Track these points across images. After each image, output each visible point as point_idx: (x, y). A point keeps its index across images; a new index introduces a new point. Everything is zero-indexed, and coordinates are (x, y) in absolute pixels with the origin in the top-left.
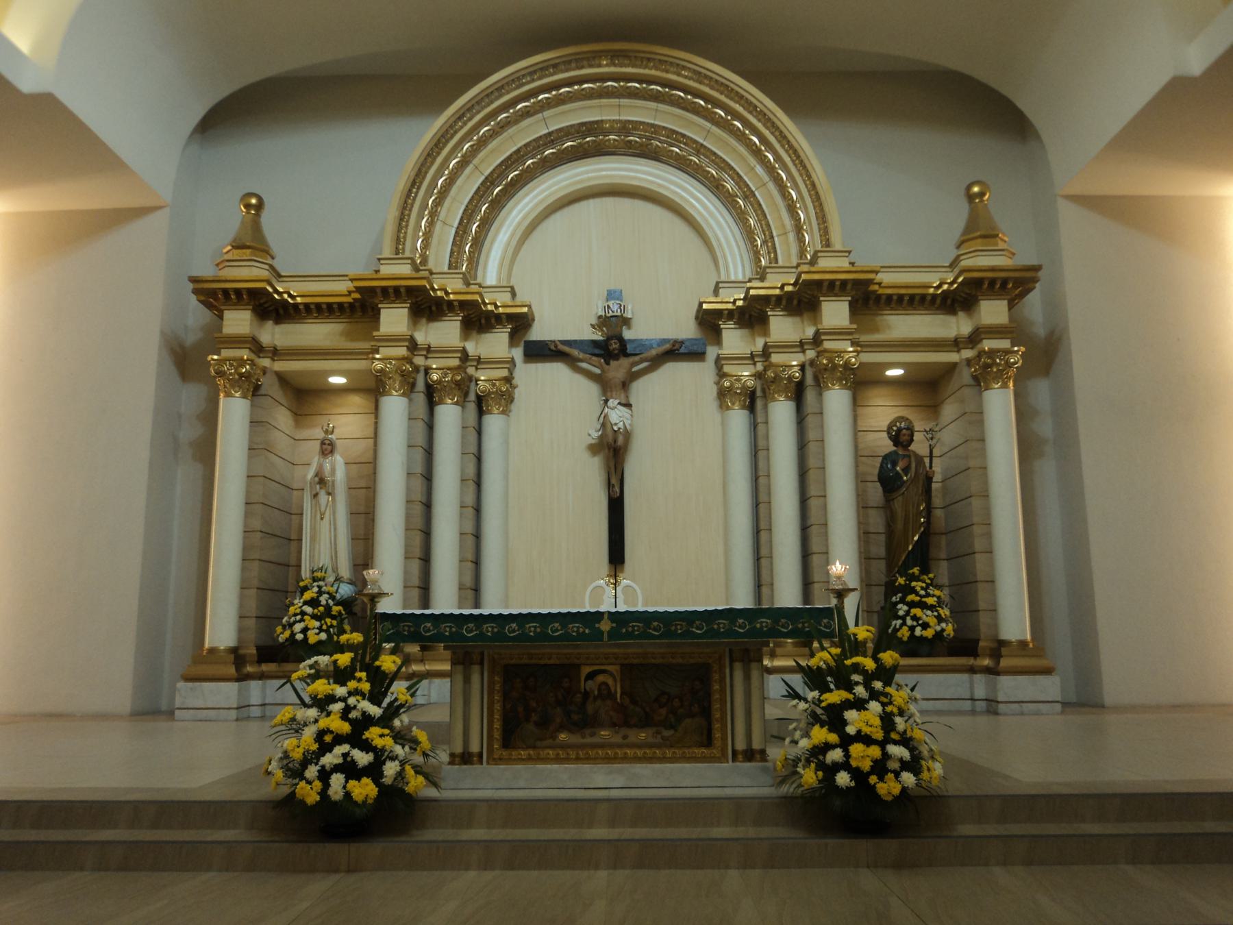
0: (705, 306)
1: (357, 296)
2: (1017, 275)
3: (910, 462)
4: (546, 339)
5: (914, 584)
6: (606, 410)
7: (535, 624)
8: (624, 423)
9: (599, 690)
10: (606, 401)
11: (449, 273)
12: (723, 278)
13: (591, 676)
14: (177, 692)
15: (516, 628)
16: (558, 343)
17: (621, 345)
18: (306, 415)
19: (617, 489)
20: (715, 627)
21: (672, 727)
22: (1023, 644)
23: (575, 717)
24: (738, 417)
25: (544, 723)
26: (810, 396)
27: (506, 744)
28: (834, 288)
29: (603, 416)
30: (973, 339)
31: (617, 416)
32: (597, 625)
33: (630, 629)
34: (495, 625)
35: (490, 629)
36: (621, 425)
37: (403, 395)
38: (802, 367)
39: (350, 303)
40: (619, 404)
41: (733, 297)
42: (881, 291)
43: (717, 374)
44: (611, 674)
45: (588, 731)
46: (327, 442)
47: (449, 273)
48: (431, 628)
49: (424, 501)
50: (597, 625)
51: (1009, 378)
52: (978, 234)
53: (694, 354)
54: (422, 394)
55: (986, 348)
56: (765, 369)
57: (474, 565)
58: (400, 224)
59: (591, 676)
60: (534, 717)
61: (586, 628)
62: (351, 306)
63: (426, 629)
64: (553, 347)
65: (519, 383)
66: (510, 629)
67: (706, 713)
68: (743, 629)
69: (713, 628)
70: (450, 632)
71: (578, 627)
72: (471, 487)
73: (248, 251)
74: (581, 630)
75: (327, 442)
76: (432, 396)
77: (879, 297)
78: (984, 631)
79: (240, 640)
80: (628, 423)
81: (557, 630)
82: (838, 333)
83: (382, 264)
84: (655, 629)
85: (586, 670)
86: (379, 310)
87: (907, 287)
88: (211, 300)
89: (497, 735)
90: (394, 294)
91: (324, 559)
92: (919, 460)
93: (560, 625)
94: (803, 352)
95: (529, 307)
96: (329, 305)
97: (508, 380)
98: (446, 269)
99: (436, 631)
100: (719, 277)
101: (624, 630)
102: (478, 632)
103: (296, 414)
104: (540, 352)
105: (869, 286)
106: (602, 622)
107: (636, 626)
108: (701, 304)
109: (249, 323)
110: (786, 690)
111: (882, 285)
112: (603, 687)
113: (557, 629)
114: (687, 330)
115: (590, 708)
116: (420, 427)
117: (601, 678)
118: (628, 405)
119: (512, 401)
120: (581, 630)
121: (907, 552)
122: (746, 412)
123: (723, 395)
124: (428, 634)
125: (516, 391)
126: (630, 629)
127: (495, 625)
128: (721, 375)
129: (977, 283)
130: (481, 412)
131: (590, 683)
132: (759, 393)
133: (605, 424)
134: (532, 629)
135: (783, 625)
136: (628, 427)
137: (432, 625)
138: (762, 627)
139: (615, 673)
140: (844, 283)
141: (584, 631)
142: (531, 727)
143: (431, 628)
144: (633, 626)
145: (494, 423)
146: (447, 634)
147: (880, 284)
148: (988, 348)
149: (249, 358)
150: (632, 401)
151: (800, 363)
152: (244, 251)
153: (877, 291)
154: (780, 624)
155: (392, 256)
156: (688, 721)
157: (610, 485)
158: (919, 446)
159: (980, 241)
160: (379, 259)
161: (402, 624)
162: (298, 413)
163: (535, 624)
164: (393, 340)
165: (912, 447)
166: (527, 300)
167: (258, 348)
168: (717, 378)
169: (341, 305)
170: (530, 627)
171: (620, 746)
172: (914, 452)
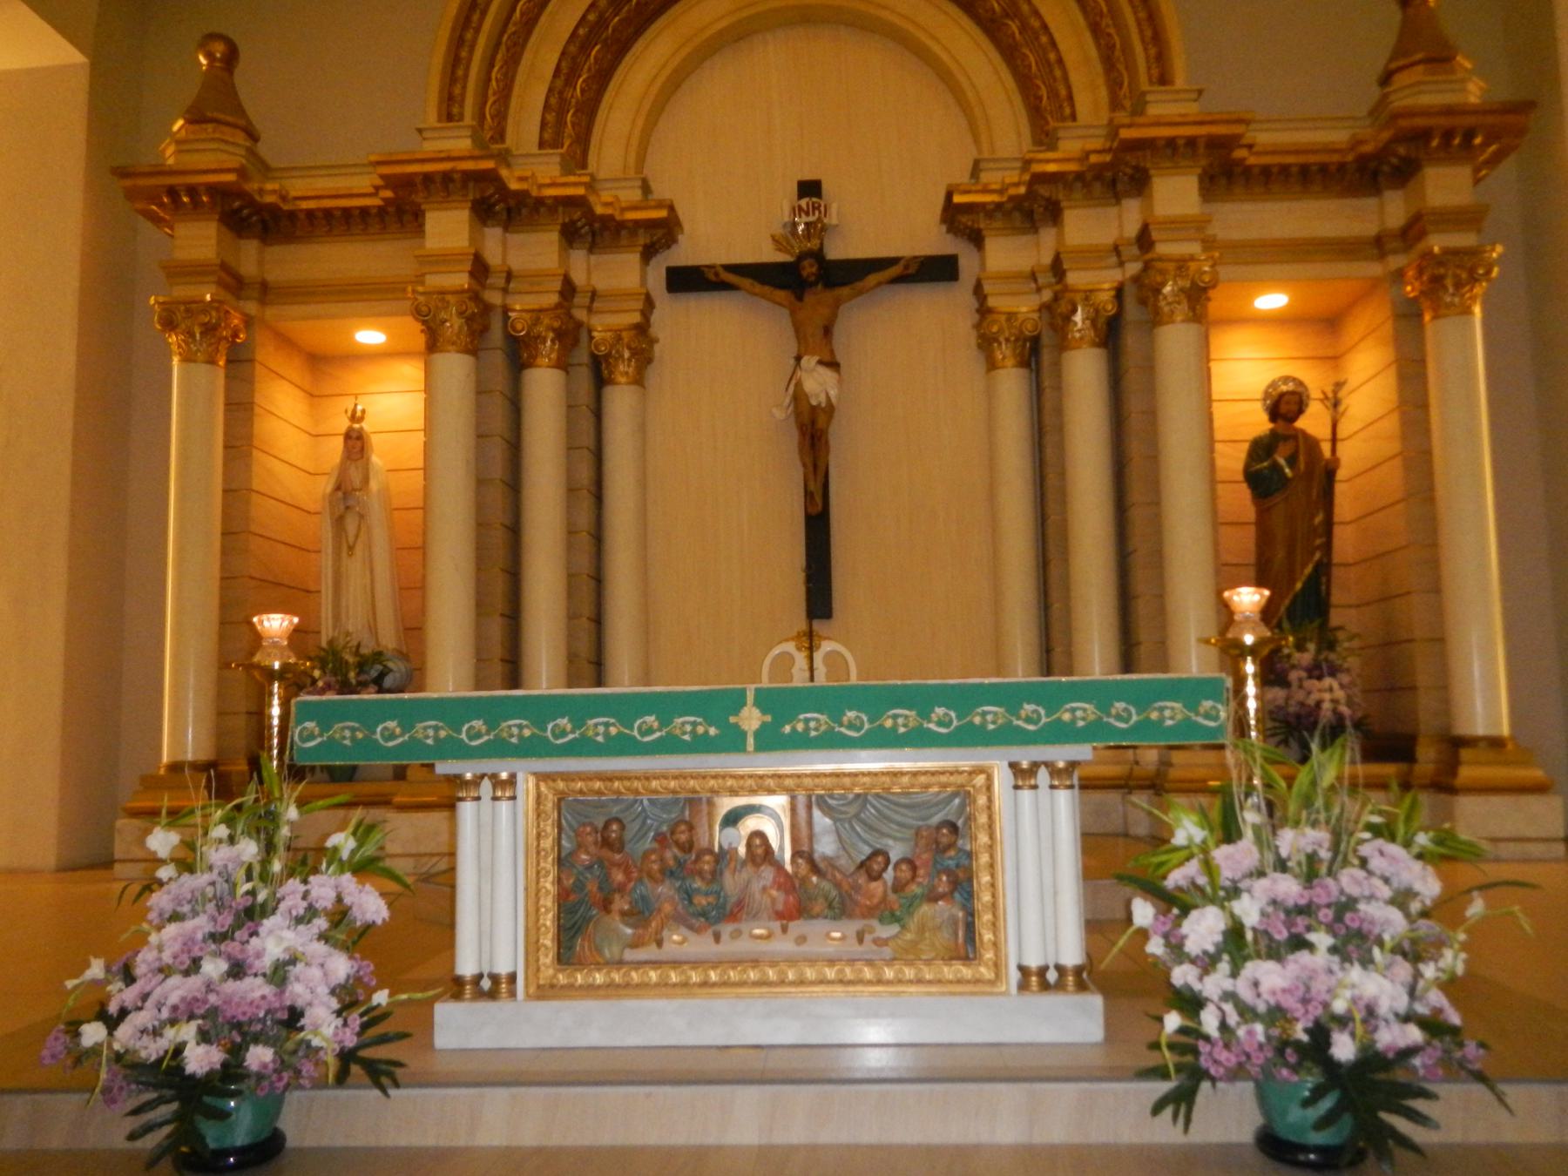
0: (957, 199)
1: (388, 194)
2: (1490, 120)
3: (1297, 447)
4: (700, 263)
5: (615, 797)
6: (799, 373)
7: (605, 719)
8: (827, 394)
9: (749, 845)
10: (798, 359)
11: (540, 155)
12: (986, 155)
13: (733, 818)
14: (116, 835)
15: (569, 727)
16: (721, 271)
17: (820, 268)
18: (327, 396)
19: (818, 499)
20: (977, 720)
21: (894, 918)
22: (1496, 743)
23: (701, 901)
24: (1011, 384)
25: (640, 914)
26: (1131, 340)
27: (566, 956)
28: (1174, 150)
29: (793, 382)
30: (1412, 232)
31: (818, 383)
32: (732, 720)
33: (800, 727)
34: (357, 725)
35: (515, 731)
36: (823, 399)
37: (467, 351)
38: (1119, 292)
39: (379, 207)
40: (820, 362)
41: (1005, 179)
42: (1252, 160)
43: (978, 311)
44: (774, 815)
45: (727, 929)
46: (354, 435)
47: (540, 155)
48: (398, 731)
49: (507, 522)
50: (732, 720)
51: (1473, 299)
52: (1419, 56)
53: (939, 270)
54: (499, 352)
55: (1436, 249)
56: (1056, 298)
57: (593, 625)
58: (453, 72)
59: (733, 818)
60: (620, 903)
61: (710, 726)
62: (382, 211)
63: (472, 732)
64: (711, 277)
65: (661, 336)
66: (557, 732)
67: (961, 884)
68: (1127, 723)
69: (971, 723)
70: (436, 738)
71: (694, 724)
72: (586, 504)
73: (210, 127)
74: (700, 730)
75: (354, 435)
76: (519, 354)
77: (1248, 170)
78: (1427, 723)
79: (220, 750)
80: (833, 393)
81: (650, 731)
82: (1178, 225)
83: (424, 139)
84: (851, 726)
85: (727, 804)
86: (423, 213)
87: (1297, 152)
88: (154, 207)
89: (548, 941)
90: (444, 185)
91: (355, 623)
92: (1312, 444)
93: (318, 724)
94: (1121, 264)
95: (671, 208)
96: (347, 212)
97: (642, 329)
98: (535, 150)
99: (406, 737)
100: (980, 151)
101: (787, 729)
102: (492, 737)
103: (312, 395)
104: (686, 280)
105: (1232, 150)
106: (745, 712)
107: (813, 719)
108: (949, 195)
109: (213, 242)
110: (1436, 1127)
111: (1255, 150)
112: (758, 841)
113: (312, 732)
114: (931, 240)
115: (731, 883)
116: (498, 409)
117: (751, 824)
118: (833, 365)
119: (650, 361)
120: (700, 730)
121: (1290, 597)
122: (1023, 372)
123: (986, 343)
124: (391, 744)
125: (657, 348)
126: (800, 727)
127: (357, 725)
128: (984, 311)
129: (1421, 136)
130: (601, 379)
131: (730, 831)
132: (1046, 340)
133: (799, 397)
134: (688, 728)
135: (850, 721)
136: (834, 400)
137: (399, 725)
138: (1074, 720)
139: (779, 812)
140: (1191, 142)
141: (706, 732)
142: (615, 921)
143: (398, 731)
144: (807, 721)
145: (621, 401)
146: (430, 742)
147: (1250, 147)
148: (1441, 248)
149: (216, 298)
150: (839, 358)
151: (1115, 285)
152: (204, 126)
153: (1245, 159)
154: (845, 719)
155: (439, 125)
156: (926, 909)
157: (808, 495)
158: (1313, 422)
159: (1420, 68)
160: (420, 131)
161: (681, 720)
162: (317, 393)
163: (605, 719)
164: (443, 260)
165: (1301, 423)
166: (667, 196)
167: (234, 283)
168: (977, 317)
169: (364, 211)
170: (596, 725)
171: (792, 961)
172: (1304, 433)
